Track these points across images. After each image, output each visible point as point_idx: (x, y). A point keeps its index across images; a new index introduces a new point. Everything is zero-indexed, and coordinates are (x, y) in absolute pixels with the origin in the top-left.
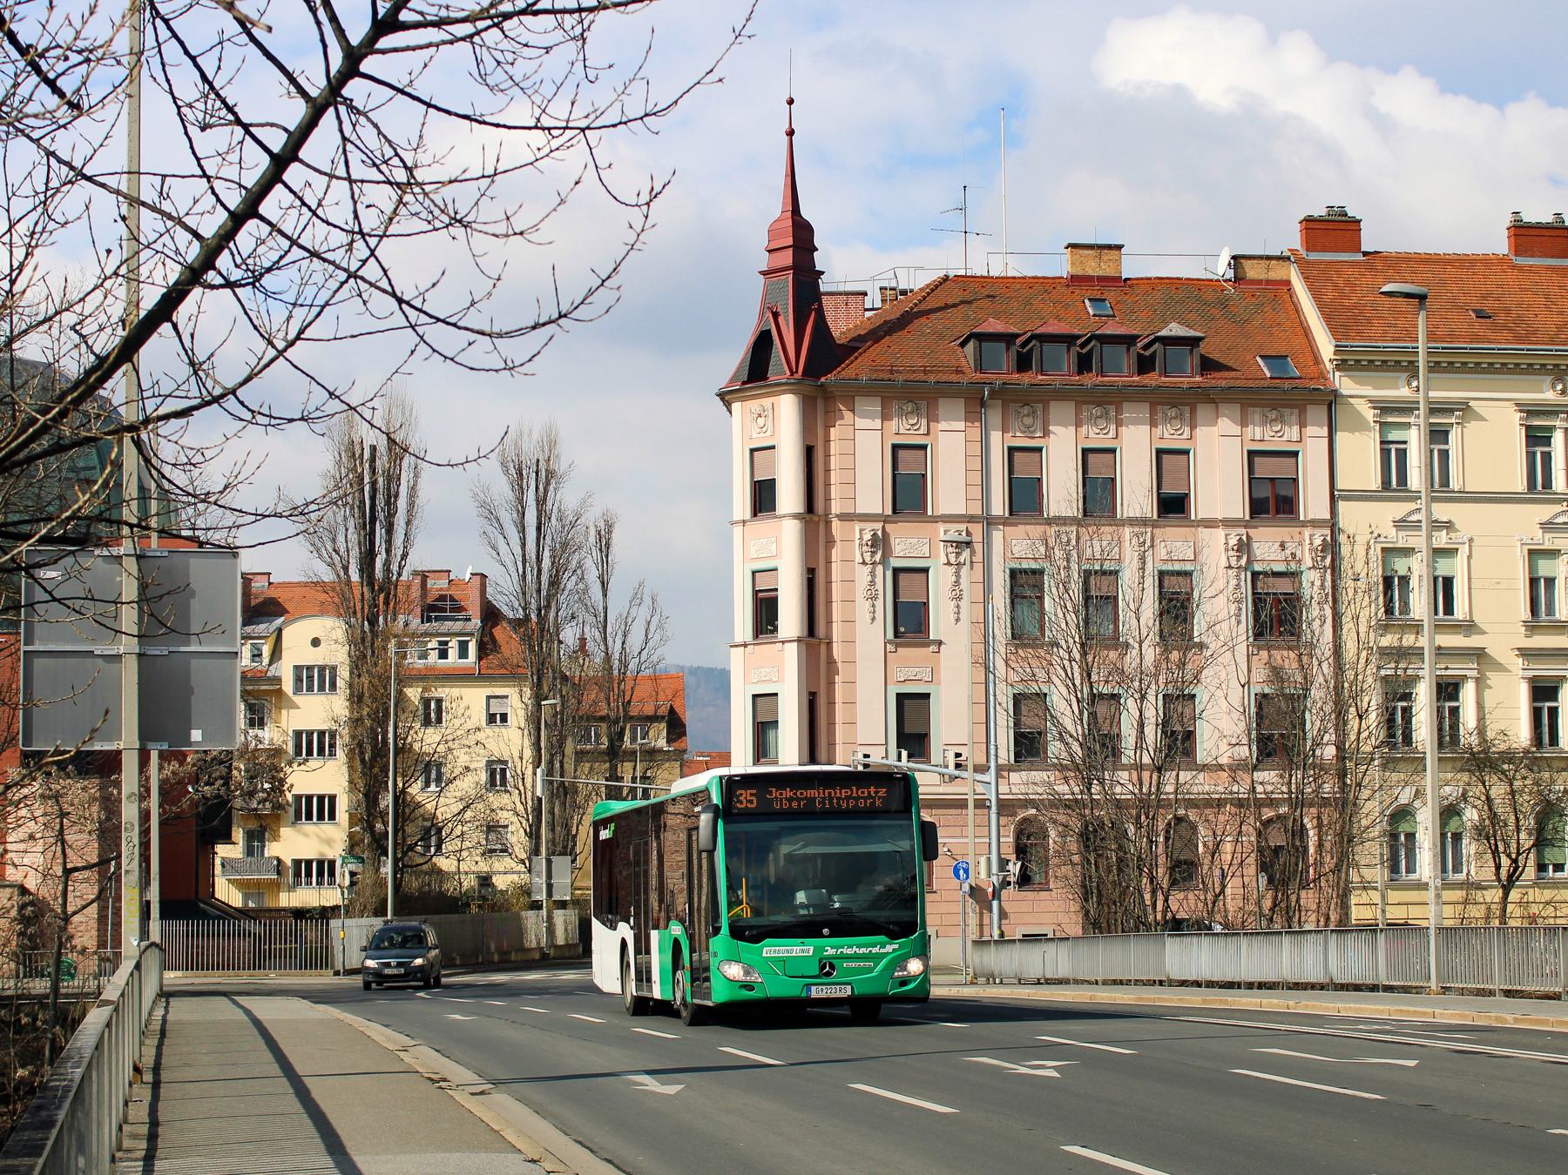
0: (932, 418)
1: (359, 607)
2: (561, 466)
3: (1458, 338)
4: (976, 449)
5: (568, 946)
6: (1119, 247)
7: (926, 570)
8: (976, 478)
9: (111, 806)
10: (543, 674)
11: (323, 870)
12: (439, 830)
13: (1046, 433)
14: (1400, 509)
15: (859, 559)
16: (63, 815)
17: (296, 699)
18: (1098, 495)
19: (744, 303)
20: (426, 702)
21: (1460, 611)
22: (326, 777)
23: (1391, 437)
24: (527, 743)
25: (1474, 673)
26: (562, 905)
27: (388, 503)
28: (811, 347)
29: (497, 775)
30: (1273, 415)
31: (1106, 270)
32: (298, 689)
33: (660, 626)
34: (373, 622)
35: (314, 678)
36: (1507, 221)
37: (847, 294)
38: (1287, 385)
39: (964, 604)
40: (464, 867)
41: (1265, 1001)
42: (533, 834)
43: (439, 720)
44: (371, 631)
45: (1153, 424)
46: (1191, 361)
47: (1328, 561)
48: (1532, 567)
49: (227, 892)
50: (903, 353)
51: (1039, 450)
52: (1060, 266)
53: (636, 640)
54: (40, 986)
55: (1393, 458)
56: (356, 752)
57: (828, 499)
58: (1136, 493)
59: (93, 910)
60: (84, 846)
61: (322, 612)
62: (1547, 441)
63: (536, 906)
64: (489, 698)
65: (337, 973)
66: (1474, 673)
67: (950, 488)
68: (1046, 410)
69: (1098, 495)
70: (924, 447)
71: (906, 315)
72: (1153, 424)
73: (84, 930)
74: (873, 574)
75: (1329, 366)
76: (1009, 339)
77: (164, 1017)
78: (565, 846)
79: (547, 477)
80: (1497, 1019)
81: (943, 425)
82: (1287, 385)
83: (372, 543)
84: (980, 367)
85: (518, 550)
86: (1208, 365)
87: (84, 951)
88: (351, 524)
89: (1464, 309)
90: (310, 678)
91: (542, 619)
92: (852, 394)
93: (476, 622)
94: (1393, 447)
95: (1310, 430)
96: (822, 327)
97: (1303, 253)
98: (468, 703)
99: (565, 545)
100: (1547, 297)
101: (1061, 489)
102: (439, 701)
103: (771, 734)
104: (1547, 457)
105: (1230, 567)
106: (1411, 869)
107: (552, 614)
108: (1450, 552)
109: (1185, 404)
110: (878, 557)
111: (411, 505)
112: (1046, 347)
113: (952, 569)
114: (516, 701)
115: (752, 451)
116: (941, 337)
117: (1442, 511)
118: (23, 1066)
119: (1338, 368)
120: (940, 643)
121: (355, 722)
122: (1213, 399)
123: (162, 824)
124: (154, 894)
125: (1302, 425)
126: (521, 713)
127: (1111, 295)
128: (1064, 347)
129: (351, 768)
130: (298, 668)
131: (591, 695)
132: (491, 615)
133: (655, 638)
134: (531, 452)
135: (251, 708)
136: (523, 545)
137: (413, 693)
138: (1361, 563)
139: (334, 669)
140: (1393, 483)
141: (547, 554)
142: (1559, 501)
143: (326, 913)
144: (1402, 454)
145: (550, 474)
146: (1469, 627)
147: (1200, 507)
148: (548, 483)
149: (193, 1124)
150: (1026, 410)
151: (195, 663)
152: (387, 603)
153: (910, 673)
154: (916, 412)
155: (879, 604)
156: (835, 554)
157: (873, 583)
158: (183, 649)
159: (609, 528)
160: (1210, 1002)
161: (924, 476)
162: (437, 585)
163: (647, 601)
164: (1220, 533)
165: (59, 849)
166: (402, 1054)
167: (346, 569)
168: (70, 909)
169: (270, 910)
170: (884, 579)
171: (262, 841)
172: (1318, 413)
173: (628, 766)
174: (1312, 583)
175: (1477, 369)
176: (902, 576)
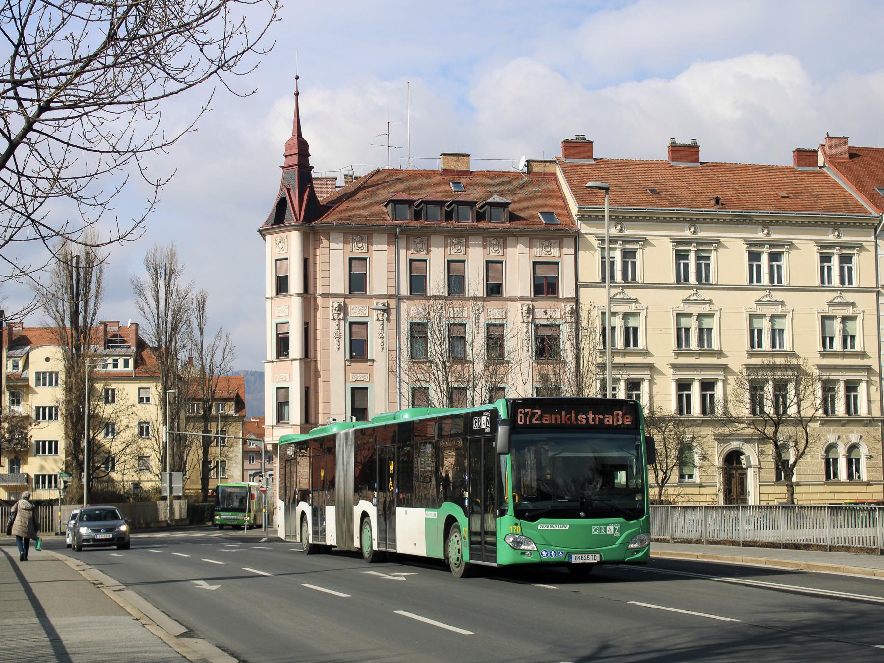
0: (370, 243)
1: (70, 341)
2: (178, 267)
3: (639, 203)
5: (181, 519)
6: (468, 155)
7: (366, 323)
10: (168, 376)
13: (429, 251)
18: (456, 284)
20: (107, 391)
21: (641, 345)
22: (53, 430)
24: (160, 412)
26: (179, 498)
27: (86, 286)
28: (307, 206)
29: (144, 429)
32: (37, 385)
33: (231, 351)
34: (78, 349)
36: (668, 143)
37: (326, 178)
38: (553, 228)
42: (163, 461)
43: (113, 401)
48: (678, 322)
50: (355, 210)
52: (438, 165)
53: (218, 358)
55: (607, 267)
56: (69, 417)
57: (315, 286)
61: (51, 343)
62: (686, 257)
63: (164, 498)
64: (140, 389)
65: (57, 534)
68: (429, 240)
69: (456, 284)
71: (358, 188)
74: (339, 325)
75: (575, 218)
76: (410, 203)
78: (180, 466)
79: (171, 273)
84: (395, 218)
85: (155, 311)
86: (513, 217)
90: (44, 378)
92: (328, 232)
96: (313, 195)
97: (563, 159)
99: (180, 309)
101: (437, 282)
102: (113, 391)
103: (286, 408)
104: (686, 266)
105: (523, 322)
107: (173, 345)
109: (502, 238)
110: (341, 316)
111: (98, 286)
114: (154, 390)
115: (276, 261)
119: (580, 219)
120: (374, 361)
121: (68, 402)
125: (561, 247)
126: (157, 397)
127: (463, 180)
129: (66, 426)
130: (38, 374)
131: (194, 387)
132: (141, 345)
133: (228, 357)
134: (161, 259)
135: (12, 394)
136: (158, 308)
139: (57, 374)
141: (170, 313)
143: (51, 503)
145: (172, 271)
147: (509, 290)
150: (419, 240)
152: (85, 339)
153: (358, 376)
155: (342, 341)
157: (339, 329)
161: (366, 274)
162: (112, 329)
166: (81, 572)
167: (63, 321)
170: (344, 328)
173: (214, 424)
174: (566, 331)
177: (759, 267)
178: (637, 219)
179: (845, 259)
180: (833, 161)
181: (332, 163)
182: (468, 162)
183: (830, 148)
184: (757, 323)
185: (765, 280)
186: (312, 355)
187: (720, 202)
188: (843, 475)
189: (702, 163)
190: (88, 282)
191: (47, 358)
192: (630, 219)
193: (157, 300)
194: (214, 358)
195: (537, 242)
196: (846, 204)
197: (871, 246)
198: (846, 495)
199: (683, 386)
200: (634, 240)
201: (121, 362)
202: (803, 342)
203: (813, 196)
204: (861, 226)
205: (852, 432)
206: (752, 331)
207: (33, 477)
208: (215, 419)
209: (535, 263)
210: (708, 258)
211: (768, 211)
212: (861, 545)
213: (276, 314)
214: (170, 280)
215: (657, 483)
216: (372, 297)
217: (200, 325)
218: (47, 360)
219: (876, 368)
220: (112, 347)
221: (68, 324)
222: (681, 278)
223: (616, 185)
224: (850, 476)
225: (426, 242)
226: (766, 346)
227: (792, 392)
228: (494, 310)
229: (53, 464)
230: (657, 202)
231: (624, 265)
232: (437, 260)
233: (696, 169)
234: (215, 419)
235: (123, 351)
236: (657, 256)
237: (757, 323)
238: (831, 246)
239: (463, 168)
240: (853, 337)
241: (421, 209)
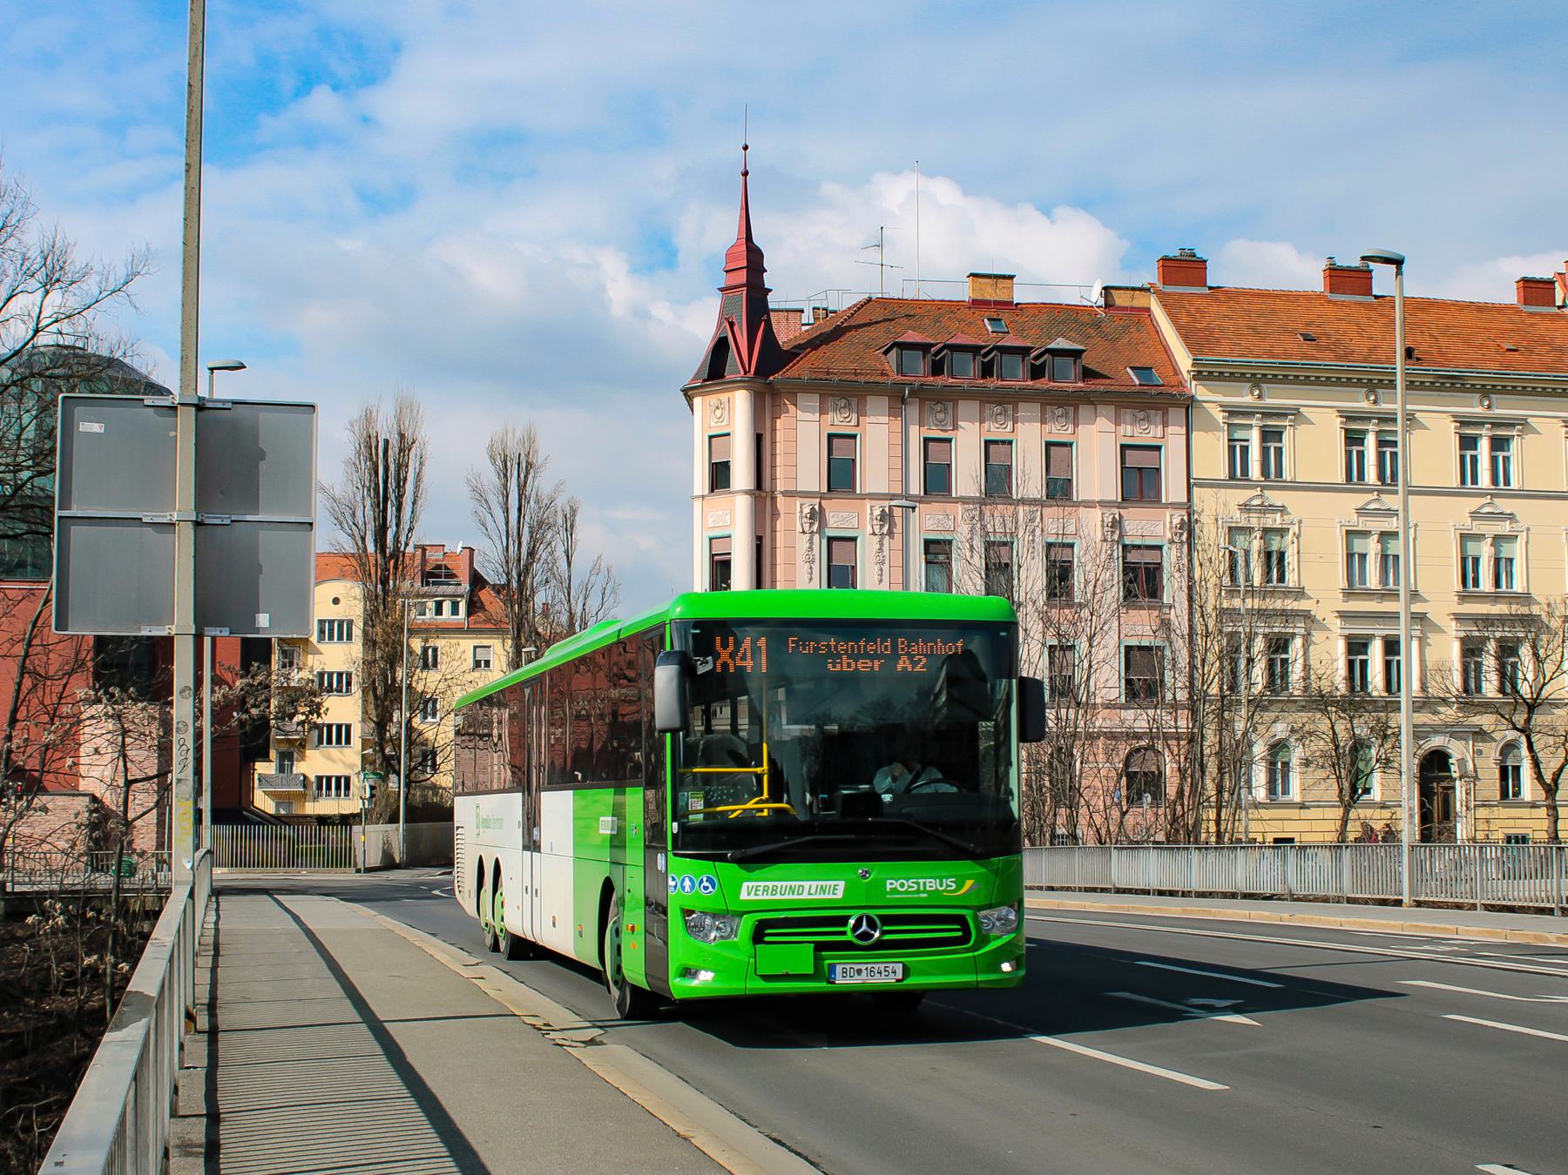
0: (861, 413)
2: (539, 459)
3: (1290, 356)
6: (1011, 277)
8: (898, 463)
9: (166, 724)
11: (342, 785)
12: (434, 754)
13: (955, 427)
14: (1243, 495)
16: (125, 733)
17: (320, 646)
18: (998, 481)
19: (699, 322)
20: (425, 650)
21: (1291, 579)
22: (344, 709)
23: (1236, 436)
25: (1302, 631)
27: (398, 486)
28: (761, 352)
30: (1141, 415)
31: (1001, 296)
32: (321, 638)
33: (614, 592)
34: (384, 582)
35: (335, 630)
38: (1153, 391)
39: (886, 568)
41: (1254, 913)
43: (435, 664)
44: (383, 589)
45: (1043, 422)
46: (1070, 367)
47: (1184, 537)
48: (1349, 545)
49: (263, 801)
50: (839, 359)
51: (949, 441)
52: (964, 293)
54: (104, 881)
55: (1237, 452)
56: (369, 689)
57: (773, 479)
58: (1029, 478)
59: (152, 817)
60: (144, 760)
61: (342, 576)
62: (1361, 442)
65: (358, 871)
66: (1302, 631)
69: (998, 481)
72: (1043, 422)
73: (144, 838)
74: (811, 541)
76: (924, 348)
77: (216, 923)
79: (528, 467)
80: (1537, 938)
81: (868, 420)
82: (1153, 391)
83: (385, 518)
84: (900, 371)
85: (503, 527)
86: (1088, 374)
87: (142, 854)
88: (368, 503)
89: (1293, 333)
91: (521, 584)
92: (795, 390)
93: (465, 587)
94: (1238, 445)
95: (1170, 429)
96: (769, 335)
97: (1160, 286)
98: (457, 652)
99: (541, 523)
100: (1358, 325)
101: (967, 476)
102: (435, 650)
104: (1361, 455)
105: (1105, 540)
106: (1286, 791)
107: (529, 581)
108: (1282, 532)
109: (1069, 404)
110: (815, 528)
111: (417, 487)
112: (956, 355)
113: (877, 539)
115: (711, 437)
116: (867, 346)
117: (1276, 498)
118: (88, 954)
121: (368, 664)
122: (1091, 400)
123: (213, 741)
124: (206, 803)
125: (1165, 425)
126: (504, 659)
127: (1005, 316)
128: (970, 356)
129: (365, 701)
130: (322, 622)
132: (477, 581)
133: (610, 601)
134: (514, 447)
135: (284, 653)
137: (417, 644)
138: (1211, 535)
139: (350, 623)
140: (1237, 475)
142: (1371, 491)
143: (346, 820)
144: (1245, 450)
145: (529, 465)
146: (1300, 593)
147: (1081, 491)
148: (527, 473)
149: (264, 1118)
150: (939, 407)
151: (265, 535)
152: (396, 568)
154: (848, 407)
155: (816, 566)
156: (779, 524)
157: (811, 548)
158: (249, 518)
159: (574, 511)
160: (1191, 912)
161: (854, 461)
162: (434, 557)
164: (1098, 512)
165: (121, 763)
167: (363, 539)
168: (131, 815)
169: (299, 817)
171: (291, 759)
172: (1177, 414)
174: (1171, 558)
175: (1307, 381)
176: (835, 544)
177: (1474, 459)
178: (1285, 380)
181: (814, 275)
184: (1472, 548)
185: (1484, 479)
187: (1416, 353)
189: (1376, 297)
190: (401, 483)
191: (337, 598)
192: (1275, 379)
193: (506, 511)
195: (1127, 414)
199: (1357, 646)
201: (447, 606)
203: (1554, 350)
206: (1464, 560)
207: (313, 779)
209: (1124, 447)
210: (1395, 444)
213: (711, 523)
215: (1342, 800)
216: (863, 497)
217: (567, 553)
218: (336, 601)
220: (434, 583)
221: (371, 548)
222: (1354, 475)
223: (1249, 328)
225: (950, 410)
226: (1486, 584)
227: (569, 761)
228: (1053, 522)
229: (344, 760)
230: (1314, 352)
231: (1265, 452)
232: (966, 445)
233: (1368, 306)
235: (450, 589)
236: (1315, 444)
237: (1472, 548)
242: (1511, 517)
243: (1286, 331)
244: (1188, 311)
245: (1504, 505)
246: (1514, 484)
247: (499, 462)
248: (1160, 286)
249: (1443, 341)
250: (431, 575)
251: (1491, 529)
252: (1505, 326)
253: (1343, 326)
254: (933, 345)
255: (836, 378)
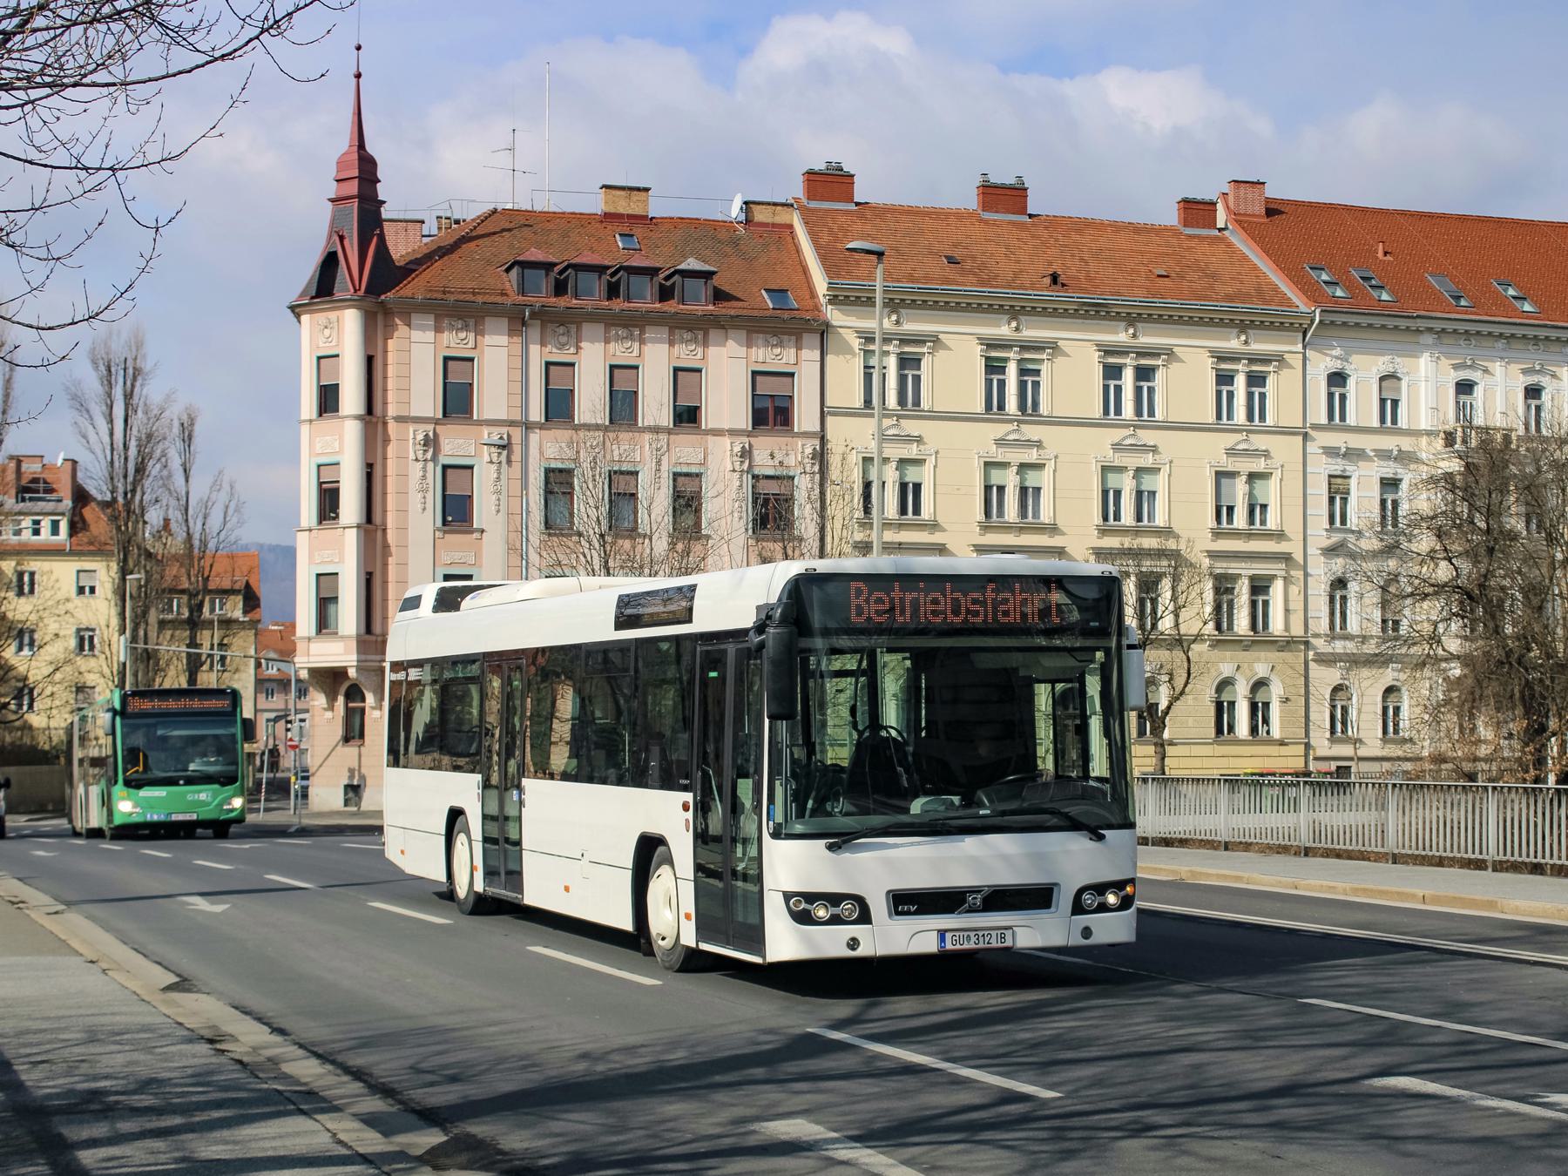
0: (479, 332)
2: (147, 366)
3: (928, 279)
4: (518, 363)
6: (647, 190)
7: (471, 467)
8: (517, 388)
12: (31, 691)
15: (412, 456)
18: (623, 406)
20: (20, 575)
28: (373, 266)
29: (85, 641)
31: (635, 209)
36: (978, 181)
38: (786, 315)
39: (503, 498)
40: (53, 724)
43: (32, 591)
47: (816, 468)
50: (452, 276)
52: (595, 204)
57: (385, 403)
58: (655, 405)
62: (1002, 370)
67: (494, 395)
69: (623, 406)
70: (472, 360)
71: (461, 239)
74: (424, 469)
75: (823, 300)
76: (548, 267)
82: (786, 315)
84: (522, 291)
85: (107, 439)
86: (719, 296)
91: (128, 503)
92: (408, 311)
93: (68, 503)
97: (805, 201)
99: (149, 436)
101: (591, 400)
102: (32, 574)
103: (332, 608)
104: (1002, 384)
107: (138, 498)
109: (699, 328)
110: (429, 455)
114: (104, 573)
116: (489, 262)
119: (830, 302)
120: (483, 531)
125: (799, 348)
127: (638, 231)
131: (172, 570)
132: (81, 497)
134: (119, 350)
136: (112, 434)
146: (934, 526)
147: (708, 419)
148: (135, 379)
150: (561, 330)
153: (457, 556)
155: (430, 496)
161: (471, 385)
163: (226, 487)
164: (727, 441)
170: (434, 474)
173: (207, 633)
174: (804, 486)
175: (947, 307)
176: (449, 471)
177: (1118, 389)
178: (924, 305)
179: (1256, 380)
180: (1241, 220)
181: (447, 175)
182: (646, 202)
183: (1237, 198)
186: (377, 518)
188: (1242, 729)
194: (209, 521)
196: (1259, 290)
197: (1296, 361)
198: (1246, 760)
200: (918, 340)
201: (46, 524)
202: (1185, 513)
203: (1207, 276)
204: (1282, 327)
205: (1258, 660)
206: (1105, 493)
208: (209, 624)
210: (1037, 372)
211: (1137, 298)
212: (1516, 857)
213: (318, 449)
214: (133, 386)
216: (480, 423)
219: (1298, 557)
220: (31, 499)
222: (994, 404)
224: (1254, 730)
226: (1128, 518)
228: (685, 450)
231: (902, 380)
234: (209, 624)
235: (50, 506)
238: (1233, 358)
239: (638, 211)
240: (1264, 507)
241: (567, 278)
242: (1154, 449)
243: (931, 253)
244: (830, 230)
245: (1148, 437)
246: (1159, 415)
247: (102, 368)
248: (805, 201)
249: (1092, 266)
250: (26, 490)
251: (1133, 461)
252: (1161, 250)
253: (991, 248)
254: (555, 265)
255: (452, 298)
